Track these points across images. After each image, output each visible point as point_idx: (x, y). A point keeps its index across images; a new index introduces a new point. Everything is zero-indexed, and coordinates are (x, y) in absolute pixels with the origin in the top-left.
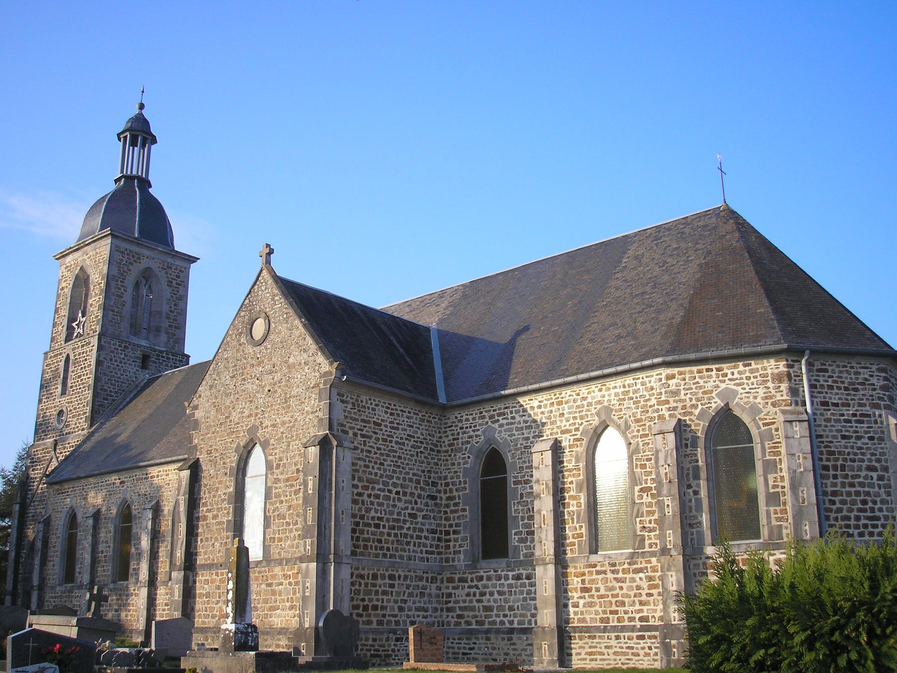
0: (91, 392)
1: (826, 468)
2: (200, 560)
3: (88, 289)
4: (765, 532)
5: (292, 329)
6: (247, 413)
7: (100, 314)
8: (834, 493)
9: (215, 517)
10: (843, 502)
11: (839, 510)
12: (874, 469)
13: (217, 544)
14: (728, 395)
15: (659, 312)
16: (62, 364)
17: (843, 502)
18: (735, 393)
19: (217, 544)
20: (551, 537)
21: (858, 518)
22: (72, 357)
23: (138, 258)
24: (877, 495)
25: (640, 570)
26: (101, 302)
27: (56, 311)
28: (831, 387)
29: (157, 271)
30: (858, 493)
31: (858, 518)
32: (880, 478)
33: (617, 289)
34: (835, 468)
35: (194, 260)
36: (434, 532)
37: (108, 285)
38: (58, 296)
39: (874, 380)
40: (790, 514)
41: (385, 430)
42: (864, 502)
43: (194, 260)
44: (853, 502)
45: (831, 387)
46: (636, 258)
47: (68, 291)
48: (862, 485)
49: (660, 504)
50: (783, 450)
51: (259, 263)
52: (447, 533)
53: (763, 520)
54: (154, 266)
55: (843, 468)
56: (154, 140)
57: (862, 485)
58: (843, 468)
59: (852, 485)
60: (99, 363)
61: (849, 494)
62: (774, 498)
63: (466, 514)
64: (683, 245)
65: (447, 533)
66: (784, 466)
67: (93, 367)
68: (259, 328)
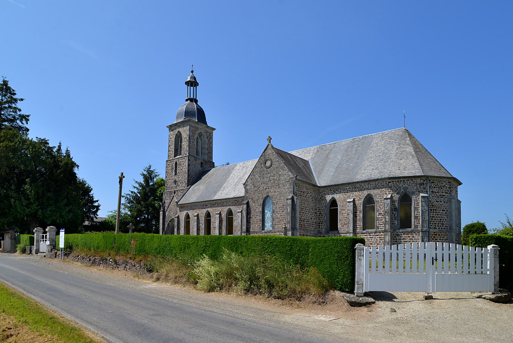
0: (187, 175)
1: (431, 210)
2: (251, 230)
3: (181, 140)
4: (413, 226)
5: (279, 162)
6: (265, 188)
7: (188, 149)
8: (433, 217)
9: (255, 218)
10: (435, 219)
11: (434, 221)
12: (444, 211)
13: (256, 225)
14: (405, 189)
15: (385, 162)
16: (174, 165)
17: (435, 219)
18: (408, 188)
19: (256, 225)
20: (352, 225)
21: (438, 224)
22: (178, 162)
23: (197, 129)
24: (444, 218)
25: (378, 235)
26: (188, 144)
27: (169, 146)
28: (435, 187)
29: (203, 133)
30: (439, 217)
31: (438, 224)
32: (446, 213)
33: (371, 153)
34: (434, 210)
35: (214, 129)
36: (316, 223)
37: (189, 138)
38: (169, 141)
39: (446, 186)
40: (421, 222)
41: (305, 194)
42: (441, 220)
43: (214, 129)
44: (438, 220)
45: (435, 187)
46: (376, 143)
47: (173, 139)
48: (440, 215)
49: (385, 218)
50: (420, 204)
51: (267, 143)
52: (319, 223)
53: (413, 223)
54: (203, 132)
55: (436, 210)
56: (198, 85)
57: (440, 215)
58: (436, 210)
59: (438, 215)
60: (189, 165)
61: (437, 217)
62: (416, 217)
63: (326, 218)
64: (391, 141)
65: (319, 223)
66: (420, 209)
67: (187, 166)
68: (268, 164)
